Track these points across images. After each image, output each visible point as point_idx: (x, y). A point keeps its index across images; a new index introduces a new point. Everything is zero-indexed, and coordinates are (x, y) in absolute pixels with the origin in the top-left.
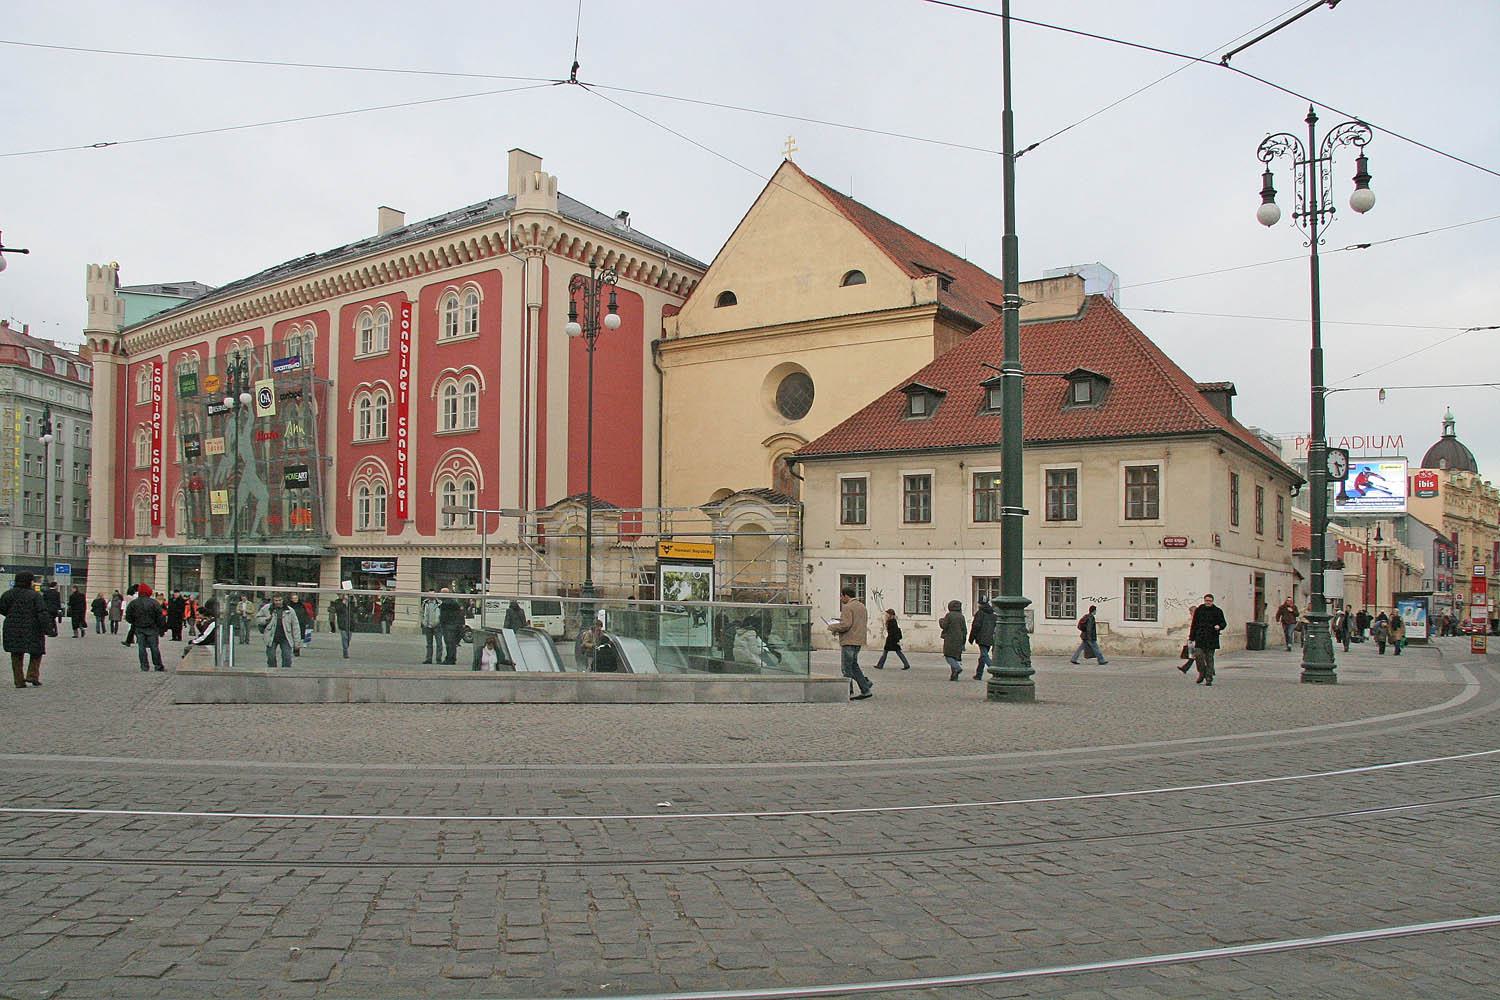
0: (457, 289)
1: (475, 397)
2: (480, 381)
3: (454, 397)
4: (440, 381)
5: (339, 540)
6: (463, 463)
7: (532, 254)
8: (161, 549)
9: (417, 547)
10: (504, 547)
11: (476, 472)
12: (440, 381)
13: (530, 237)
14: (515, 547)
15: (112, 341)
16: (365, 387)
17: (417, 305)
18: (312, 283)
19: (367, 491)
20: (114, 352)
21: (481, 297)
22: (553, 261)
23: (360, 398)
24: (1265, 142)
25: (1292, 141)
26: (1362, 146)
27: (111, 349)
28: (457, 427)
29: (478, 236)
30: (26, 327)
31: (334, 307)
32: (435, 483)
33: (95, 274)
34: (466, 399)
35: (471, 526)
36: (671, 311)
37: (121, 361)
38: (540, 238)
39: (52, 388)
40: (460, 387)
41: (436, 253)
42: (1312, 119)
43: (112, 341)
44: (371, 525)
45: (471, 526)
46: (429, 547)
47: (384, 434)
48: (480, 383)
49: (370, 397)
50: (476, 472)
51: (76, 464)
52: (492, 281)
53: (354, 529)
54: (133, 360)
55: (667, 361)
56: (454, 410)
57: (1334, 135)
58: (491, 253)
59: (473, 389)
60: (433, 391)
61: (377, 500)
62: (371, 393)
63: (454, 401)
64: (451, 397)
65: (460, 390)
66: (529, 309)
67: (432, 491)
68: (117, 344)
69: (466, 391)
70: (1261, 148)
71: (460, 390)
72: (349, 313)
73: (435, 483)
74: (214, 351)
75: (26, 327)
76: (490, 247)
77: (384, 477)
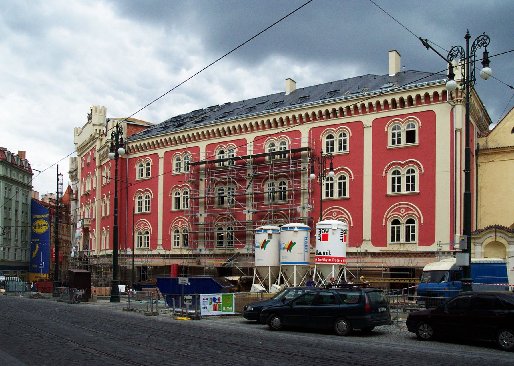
0: (276, 139)
6: (183, 222)
7: (459, 103)
16: (140, 191)
17: (163, 159)
23: (392, 169)
28: (180, 208)
29: (163, 139)
31: (161, 152)
32: (171, 230)
33: (103, 111)
41: (150, 143)
42: (468, 37)
44: (143, 246)
47: (149, 210)
48: (151, 195)
49: (142, 195)
51: (22, 212)
52: (429, 119)
53: (172, 247)
58: (155, 148)
59: (149, 197)
61: (146, 237)
63: (142, 201)
64: (140, 200)
65: (144, 198)
66: (456, 131)
67: (384, 224)
71: (144, 198)
72: (168, 155)
73: (171, 230)
74: (307, 140)
76: (163, 144)
77: (187, 225)
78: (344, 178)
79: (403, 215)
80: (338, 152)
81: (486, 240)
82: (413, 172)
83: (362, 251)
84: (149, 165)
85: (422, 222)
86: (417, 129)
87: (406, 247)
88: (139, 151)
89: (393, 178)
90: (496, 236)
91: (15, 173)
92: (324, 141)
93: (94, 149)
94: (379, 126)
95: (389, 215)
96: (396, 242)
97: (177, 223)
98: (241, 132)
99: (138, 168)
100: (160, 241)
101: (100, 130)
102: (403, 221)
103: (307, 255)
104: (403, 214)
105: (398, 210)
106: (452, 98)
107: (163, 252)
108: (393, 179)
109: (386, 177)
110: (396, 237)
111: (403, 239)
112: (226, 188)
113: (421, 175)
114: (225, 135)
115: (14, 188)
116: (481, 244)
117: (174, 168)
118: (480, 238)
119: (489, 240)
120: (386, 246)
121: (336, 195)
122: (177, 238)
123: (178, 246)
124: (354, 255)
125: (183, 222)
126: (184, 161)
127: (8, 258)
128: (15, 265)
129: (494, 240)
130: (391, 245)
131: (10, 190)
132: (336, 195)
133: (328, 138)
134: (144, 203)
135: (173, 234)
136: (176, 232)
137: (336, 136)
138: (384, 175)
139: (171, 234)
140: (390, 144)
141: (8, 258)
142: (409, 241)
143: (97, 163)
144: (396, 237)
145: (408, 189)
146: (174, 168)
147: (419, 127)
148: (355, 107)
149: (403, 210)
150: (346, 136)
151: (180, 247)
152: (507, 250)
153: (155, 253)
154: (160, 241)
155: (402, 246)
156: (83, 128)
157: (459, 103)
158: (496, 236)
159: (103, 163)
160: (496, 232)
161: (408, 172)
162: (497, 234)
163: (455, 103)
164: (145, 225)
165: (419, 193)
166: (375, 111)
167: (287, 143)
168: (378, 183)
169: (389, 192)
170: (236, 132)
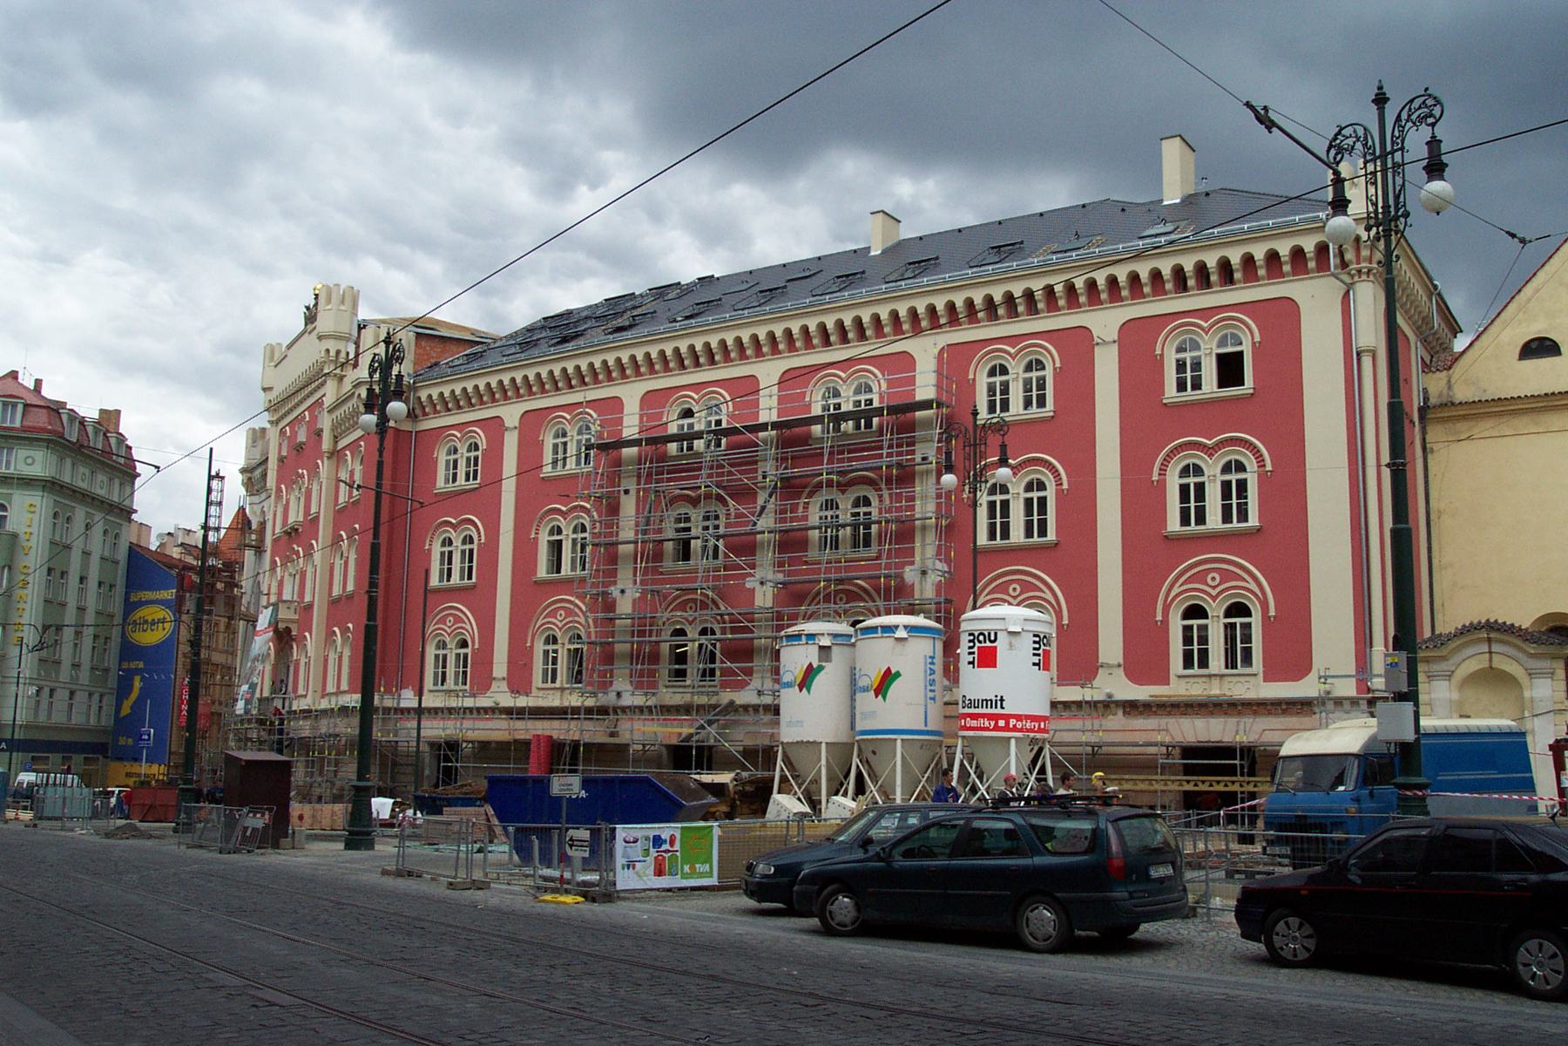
1: (1045, 498)
3: (1004, 497)
6: (569, 612)
7: (1364, 277)
17: (516, 433)
18: (481, 383)
21: (483, 445)
24: (1335, 139)
25: (1361, 132)
26: (1433, 125)
28: (563, 573)
30: (38, 383)
31: (511, 414)
34: (463, 552)
39: (29, 500)
42: (1381, 100)
51: (100, 584)
56: (450, 563)
57: (1404, 116)
58: (494, 400)
64: (447, 549)
65: (457, 542)
67: (1159, 618)
70: (1330, 147)
71: (457, 542)
72: (532, 423)
74: (635, 420)
75: (38, 383)
77: (1049, 596)
79: (1214, 593)
80: (1021, 411)
81: (1463, 666)
82: (1241, 467)
83: (1098, 696)
84: (477, 449)
87: (1226, 686)
92: (982, 381)
93: (319, 403)
94: (1137, 338)
95: (1174, 594)
96: (1196, 670)
97: (553, 614)
98: (610, 378)
99: (442, 457)
100: (500, 668)
101: (338, 352)
102: (1216, 609)
103: (935, 711)
104: (1214, 588)
106: (1344, 265)
107: (507, 701)
108: (1184, 489)
109: (1162, 484)
110: (1196, 657)
114: (697, 364)
115: (80, 514)
117: (548, 456)
118: (1444, 658)
121: (1017, 535)
124: (1074, 707)
126: (577, 438)
129: (1486, 665)
130: (1183, 681)
132: (1017, 535)
133: (992, 373)
134: (456, 558)
135: (540, 647)
136: (547, 642)
137: (1016, 371)
140: (1171, 391)
142: (1234, 666)
143: (326, 444)
144: (1196, 657)
145: (1029, 534)
146: (548, 456)
147: (1254, 343)
148: (1070, 288)
150: (1043, 368)
151: (558, 684)
152: (1527, 694)
153: (484, 702)
154: (500, 668)
155: (1216, 682)
156: (289, 347)
157: (1364, 277)
159: (341, 445)
160: (1489, 640)
161: (1226, 469)
162: (1495, 648)
164: (458, 619)
165: (474, 587)
167: (875, 389)
168: (1140, 499)
169: (1174, 524)
170: (826, 342)
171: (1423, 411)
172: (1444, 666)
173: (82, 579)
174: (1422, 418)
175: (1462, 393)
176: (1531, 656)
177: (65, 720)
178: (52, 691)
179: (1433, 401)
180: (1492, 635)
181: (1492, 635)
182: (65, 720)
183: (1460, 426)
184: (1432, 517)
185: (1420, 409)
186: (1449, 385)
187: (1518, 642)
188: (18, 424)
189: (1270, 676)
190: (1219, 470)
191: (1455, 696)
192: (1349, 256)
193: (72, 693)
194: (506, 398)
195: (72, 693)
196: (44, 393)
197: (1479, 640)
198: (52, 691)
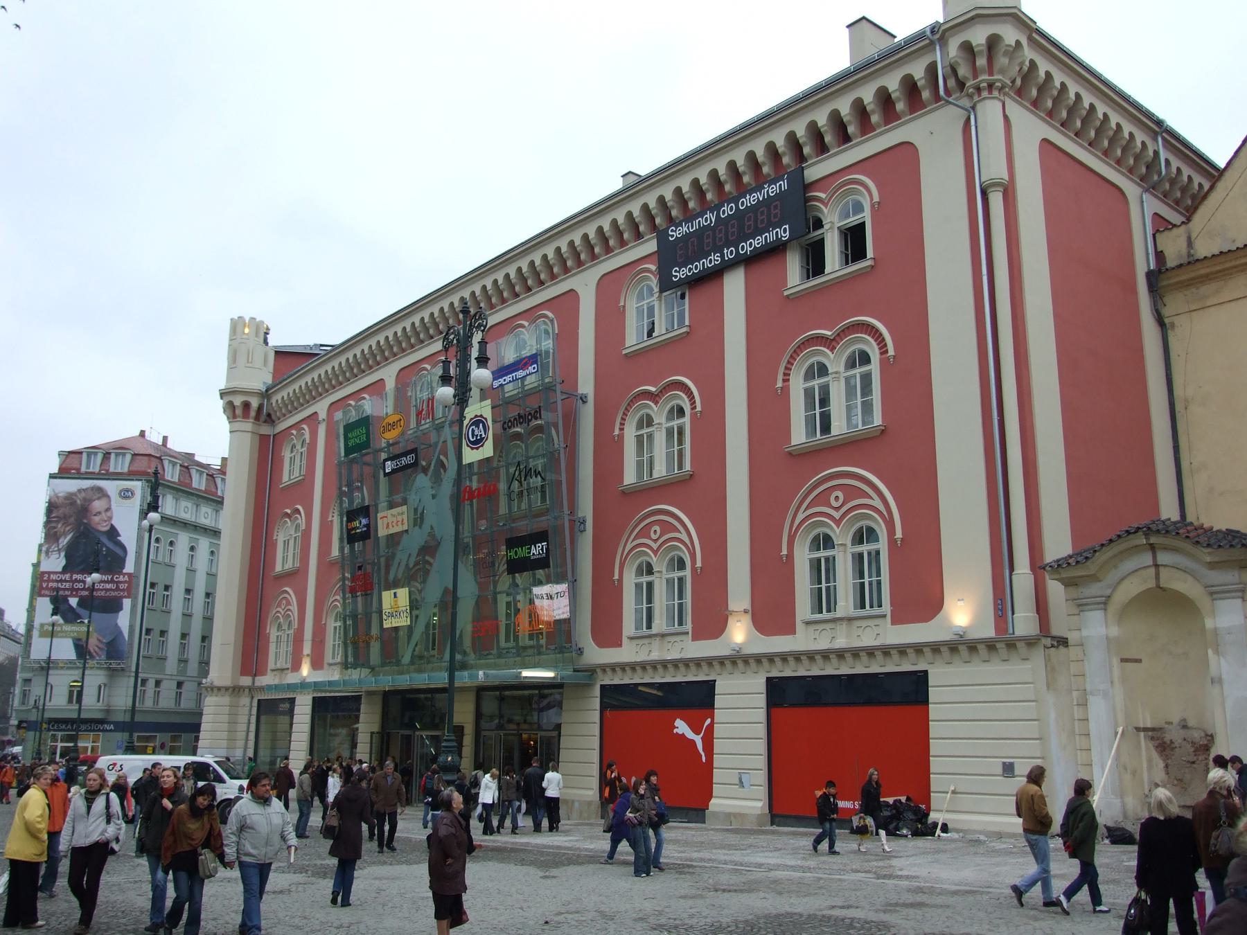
0: (526, 324)
2: (693, 403)
4: (796, 352)
5: (596, 655)
7: (985, 94)
8: (738, 660)
9: (758, 659)
10: (961, 647)
11: (882, 508)
12: (796, 352)
13: (981, 62)
14: (991, 645)
15: (255, 403)
19: (649, 566)
20: (257, 418)
22: (1020, 115)
27: (253, 414)
28: (835, 431)
30: (165, 438)
31: (585, 284)
35: (876, 611)
36: (1161, 225)
37: (266, 430)
38: (1002, 61)
40: (835, 361)
43: (255, 403)
45: (876, 611)
46: (784, 657)
50: (882, 508)
54: (281, 426)
55: (1174, 305)
60: (780, 377)
62: (832, 350)
66: (984, 194)
67: (784, 552)
68: (260, 408)
69: (670, 417)
75: (165, 438)
77: (877, 503)
78: (865, 359)
79: (837, 515)
81: (1125, 585)
85: (899, 535)
86: (867, 216)
88: (517, 295)
89: (806, 390)
90: (1156, 566)
91: (189, 505)
96: (868, 611)
104: (837, 509)
105: (823, 499)
109: (786, 390)
110: (823, 600)
111: (845, 604)
112: (835, 361)
113: (884, 363)
116: (1105, 603)
118: (1094, 578)
119: (1133, 587)
120: (791, 630)
122: (822, 571)
123: (649, 627)
125: (851, 493)
127: (156, 701)
128: (177, 720)
129: (1151, 584)
131: (171, 543)
138: (779, 384)
139: (621, 580)
141: (156, 701)
142: (863, 606)
144: (823, 600)
147: (872, 206)
149: (837, 498)
151: (655, 630)
152: (1209, 623)
155: (842, 628)
157: (996, 93)
158: (1156, 566)
160: (1153, 548)
162: (1163, 558)
163: (970, 96)
164: (668, 528)
166: (573, 268)
171: (1153, 278)
172: (1094, 590)
173: (188, 591)
174: (1153, 287)
175: (1204, 249)
176: (1212, 566)
177: (173, 705)
178: (158, 683)
179: (1171, 262)
180: (1153, 540)
181: (1153, 540)
182: (173, 705)
183: (1206, 289)
184: (1178, 407)
185: (1149, 275)
186: (1190, 244)
187: (1187, 546)
188: (126, 470)
189: (899, 618)
190: (842, 369)
191: (1114, 631)
192: (963, 71)
193: (180, 685)
194: (580, 263)
195: (180, 685)
196: (169, 446)
197: (1137, 549)
198: (158, 683)
